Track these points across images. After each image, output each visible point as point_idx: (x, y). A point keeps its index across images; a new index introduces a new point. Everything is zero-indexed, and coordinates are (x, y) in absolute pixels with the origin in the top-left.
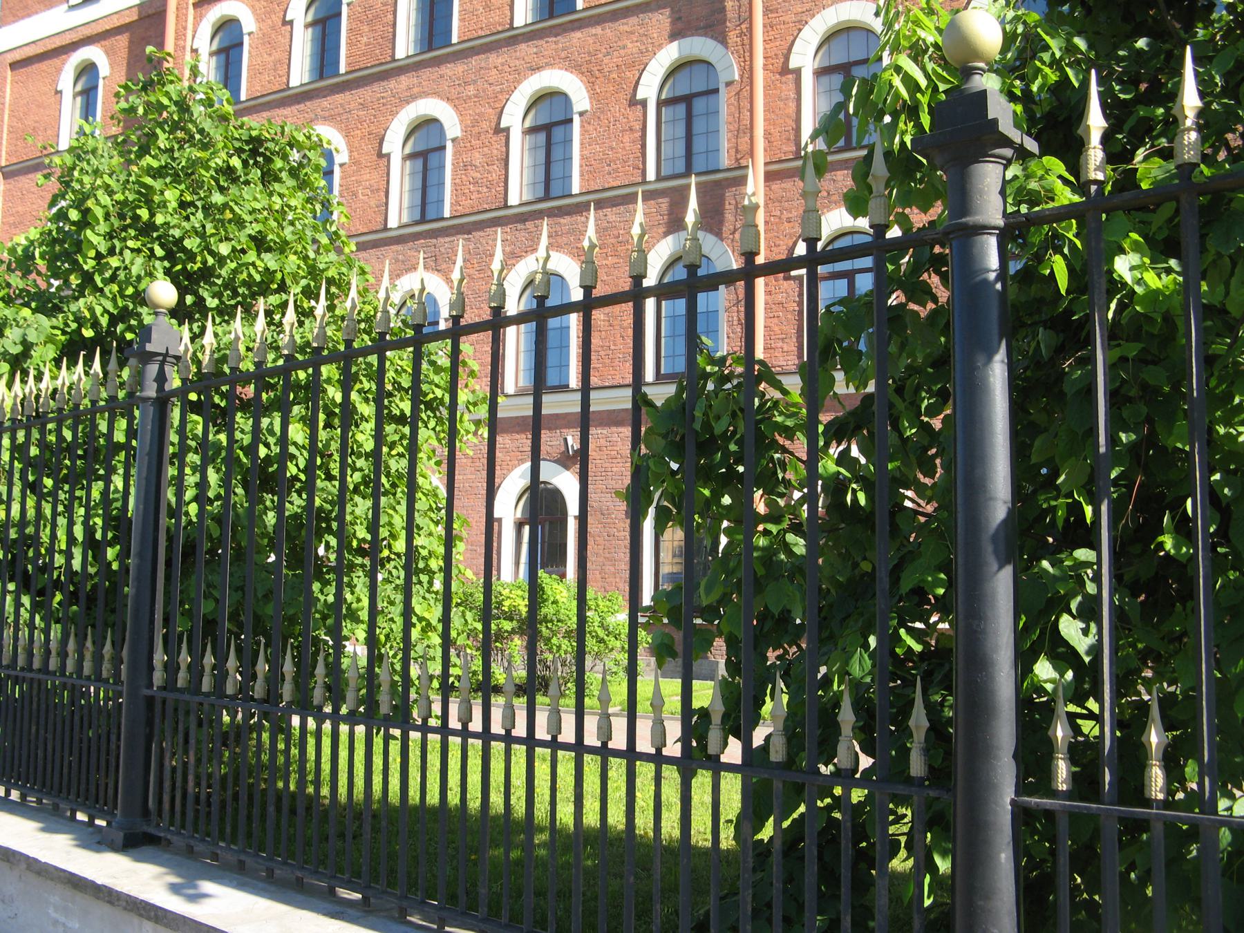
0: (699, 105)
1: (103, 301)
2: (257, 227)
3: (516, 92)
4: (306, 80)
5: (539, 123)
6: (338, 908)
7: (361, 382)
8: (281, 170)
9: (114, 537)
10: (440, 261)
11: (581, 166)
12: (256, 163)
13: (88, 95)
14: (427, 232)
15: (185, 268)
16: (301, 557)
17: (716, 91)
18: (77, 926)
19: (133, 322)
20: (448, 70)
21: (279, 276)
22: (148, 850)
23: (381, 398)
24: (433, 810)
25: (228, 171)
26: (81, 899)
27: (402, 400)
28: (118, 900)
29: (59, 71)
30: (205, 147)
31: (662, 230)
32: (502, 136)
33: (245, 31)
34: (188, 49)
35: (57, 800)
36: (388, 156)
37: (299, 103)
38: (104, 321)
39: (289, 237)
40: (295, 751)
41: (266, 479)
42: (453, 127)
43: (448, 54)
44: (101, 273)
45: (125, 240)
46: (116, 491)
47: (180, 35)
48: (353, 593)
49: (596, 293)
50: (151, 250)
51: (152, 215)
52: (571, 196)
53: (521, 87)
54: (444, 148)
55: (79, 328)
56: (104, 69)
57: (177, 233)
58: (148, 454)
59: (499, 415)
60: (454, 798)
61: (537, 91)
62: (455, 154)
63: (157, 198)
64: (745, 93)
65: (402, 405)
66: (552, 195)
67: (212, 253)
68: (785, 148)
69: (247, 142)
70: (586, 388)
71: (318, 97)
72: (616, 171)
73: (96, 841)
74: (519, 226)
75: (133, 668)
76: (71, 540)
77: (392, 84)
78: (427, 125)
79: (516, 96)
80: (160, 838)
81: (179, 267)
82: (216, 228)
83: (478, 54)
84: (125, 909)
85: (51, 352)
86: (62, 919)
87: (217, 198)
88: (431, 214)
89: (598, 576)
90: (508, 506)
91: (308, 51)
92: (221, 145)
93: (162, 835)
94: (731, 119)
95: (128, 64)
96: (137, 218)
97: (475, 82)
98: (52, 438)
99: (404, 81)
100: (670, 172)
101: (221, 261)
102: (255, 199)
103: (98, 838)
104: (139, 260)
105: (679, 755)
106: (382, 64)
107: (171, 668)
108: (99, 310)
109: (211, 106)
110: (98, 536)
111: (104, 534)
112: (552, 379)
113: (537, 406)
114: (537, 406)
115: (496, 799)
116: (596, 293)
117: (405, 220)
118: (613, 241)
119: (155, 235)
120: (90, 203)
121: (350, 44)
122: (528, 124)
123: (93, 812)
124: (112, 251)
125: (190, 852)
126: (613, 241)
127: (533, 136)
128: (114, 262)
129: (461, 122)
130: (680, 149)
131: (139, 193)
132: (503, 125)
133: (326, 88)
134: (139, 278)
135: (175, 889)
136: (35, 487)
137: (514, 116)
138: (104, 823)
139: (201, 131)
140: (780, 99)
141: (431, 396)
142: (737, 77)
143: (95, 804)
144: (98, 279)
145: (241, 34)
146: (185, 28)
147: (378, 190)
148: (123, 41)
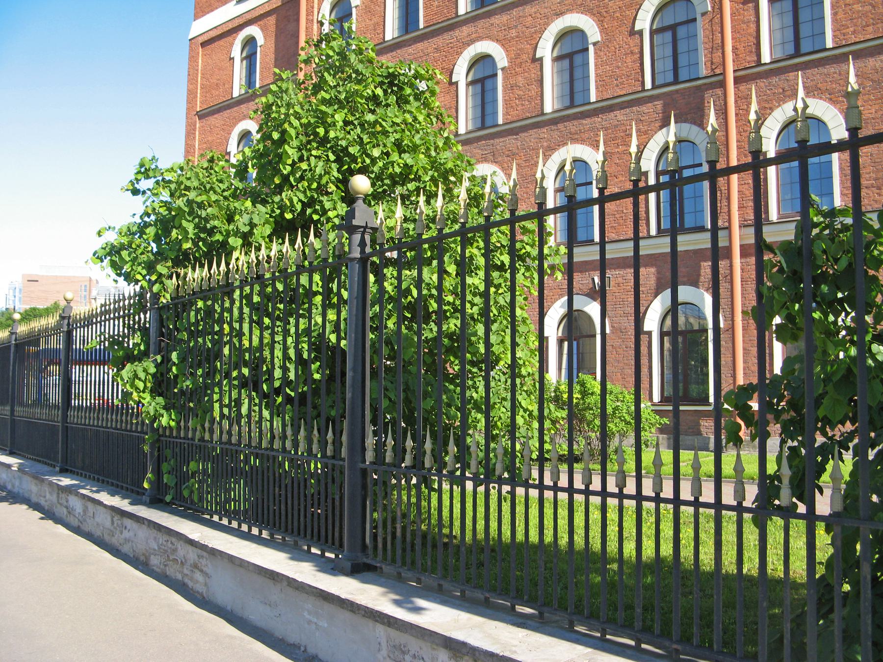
0: (682, 32)
1: (298, 193)
2: (398, 136)
3: (546, 32)
4: (396, 35)
5: (564, 53)
6: (521, 621)
7: (478, 242)
8: (409, 96)
9: (316, 357)
10: (497, 156)
11: (596, 82)
12: (392, 91)
13: (250, 59)
14: (487, 135)
15: (350, 168)
16: (436, 369)
17: (695, 20)
18: (326, 625)
19: (317, 207)
20: (496, 20)
21: (415, 169)
22: (369, 575)
23: (488, 253)
24: (534, 546)
25: (374, 98)
26: (328, 607)
27: (501, 254)
28: (359, 609)
29: (232, 45)
30: (359, 82)
31: (658, 124)
32: (537, 64)
33: (353, 5)
34: (315, 21)
35: (296, 539)
36: (456, 83)
37: (392, 51)
38: (299, 207)
39: (418, 142)
40: (424, 504)
41: (418, 312)
42: (501, 59)
43: (496, 8)
44: (294, 175)
45: (310, 150)
46: (316, 324)
47: (310, 12)
48: (477, 393)
49: (862, 134)
50: (327, 156)
51: (327, 132)
52: (590, 103)
53: (550, 28)
54: (496, 75)
55: (282, 214)
56: (260, 41)
57: (344, 143)
58: (356, 298)
59: (607, 257)
60: (548, 538)
61: (562, 30)
62: (504, 79)
63: (329, 120)
64: (717, 20)
65: (502, 258)
66: (576, 104)
67: (368, 156)
68: (748, 58)
69: (386, 77)
70: (603, 243)
71: (405, 46)
72: (622, 83)
73: (333, 568)
74: (553, 127)
75: (351, 449)
76: (286, 357)
77: (457, 33)
78: (484, 59)
79: (546, 34)
80: (376, 567)
81: (346, 167)
82: (369, 137)
83: (517, 7)
84: (364, 616)
85: (268, 230)
86: (315, 620)
87: (370, 117)
88: (488, 123)
89: (620, 377)
90: (553, 328)
91: (396, 15)
92: (370, 80)
93: (378, 565)
94: (706, 40)
95: (276, 35)
96: (316, 134)
97: (516, 27)
98: (269, 289)
99: (466, 30)
100: (662, 82)
101: (374, 161)
102: (396, 116)
103: (332, 565)
104: (321, 164)
105: (805, 512)
106: (449, 19)
107: (380, 448)
108: (295, 200)
109: (361, 54)
110: (305, 356)
111: (309, 355)
112: (581, 236)
113: (570, 255)
114: (570, 255)
115: (579, 540)
116: (862, 134)
117: (470, 128)
118: (622, 134)
119: (328, 146)
120: (286, 126)
121: (426, 7)
122: (555, 54)
123: (323, 547)
124: (301, 159)
125: (399, 578)
126: (622, 134)
127: (560, 62)
128: (304, 166)
129: (507, 56)
130: (669, 65)
131: (317, 117)
132: (537, 56)
133: (410, 39)
134: (321, 176)
135: (397, 603)
136: (260, 323)
137: (546, 49)
138: (333, 556)
139: (357, 72)
140: (744, 22)
141: (524, 251)
142: (710, 9)
143: (326, 542)
144: (292, 179)
145: (351, 8)
146: (313, 8)
147: (450, 108)
148: (272, 20)
